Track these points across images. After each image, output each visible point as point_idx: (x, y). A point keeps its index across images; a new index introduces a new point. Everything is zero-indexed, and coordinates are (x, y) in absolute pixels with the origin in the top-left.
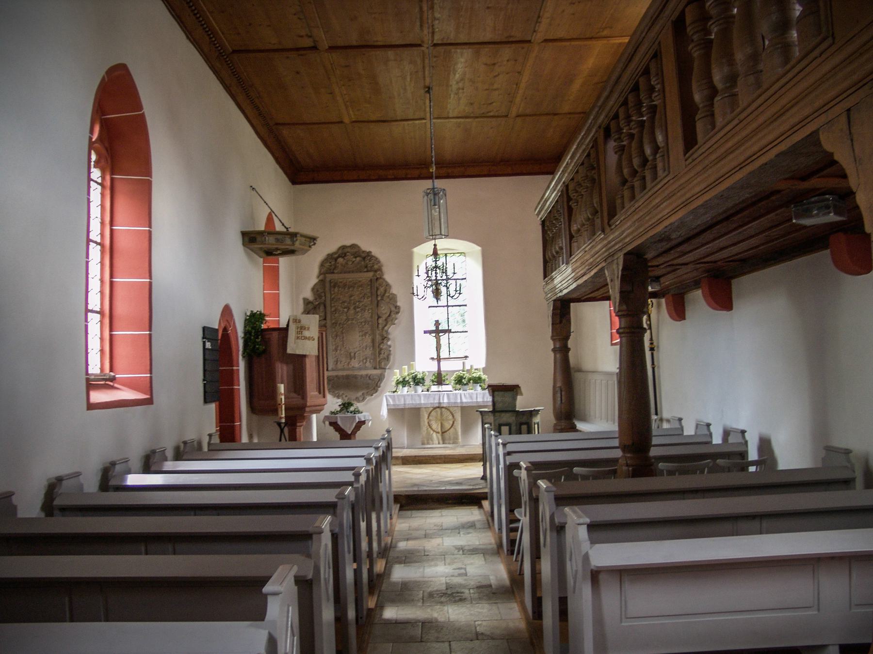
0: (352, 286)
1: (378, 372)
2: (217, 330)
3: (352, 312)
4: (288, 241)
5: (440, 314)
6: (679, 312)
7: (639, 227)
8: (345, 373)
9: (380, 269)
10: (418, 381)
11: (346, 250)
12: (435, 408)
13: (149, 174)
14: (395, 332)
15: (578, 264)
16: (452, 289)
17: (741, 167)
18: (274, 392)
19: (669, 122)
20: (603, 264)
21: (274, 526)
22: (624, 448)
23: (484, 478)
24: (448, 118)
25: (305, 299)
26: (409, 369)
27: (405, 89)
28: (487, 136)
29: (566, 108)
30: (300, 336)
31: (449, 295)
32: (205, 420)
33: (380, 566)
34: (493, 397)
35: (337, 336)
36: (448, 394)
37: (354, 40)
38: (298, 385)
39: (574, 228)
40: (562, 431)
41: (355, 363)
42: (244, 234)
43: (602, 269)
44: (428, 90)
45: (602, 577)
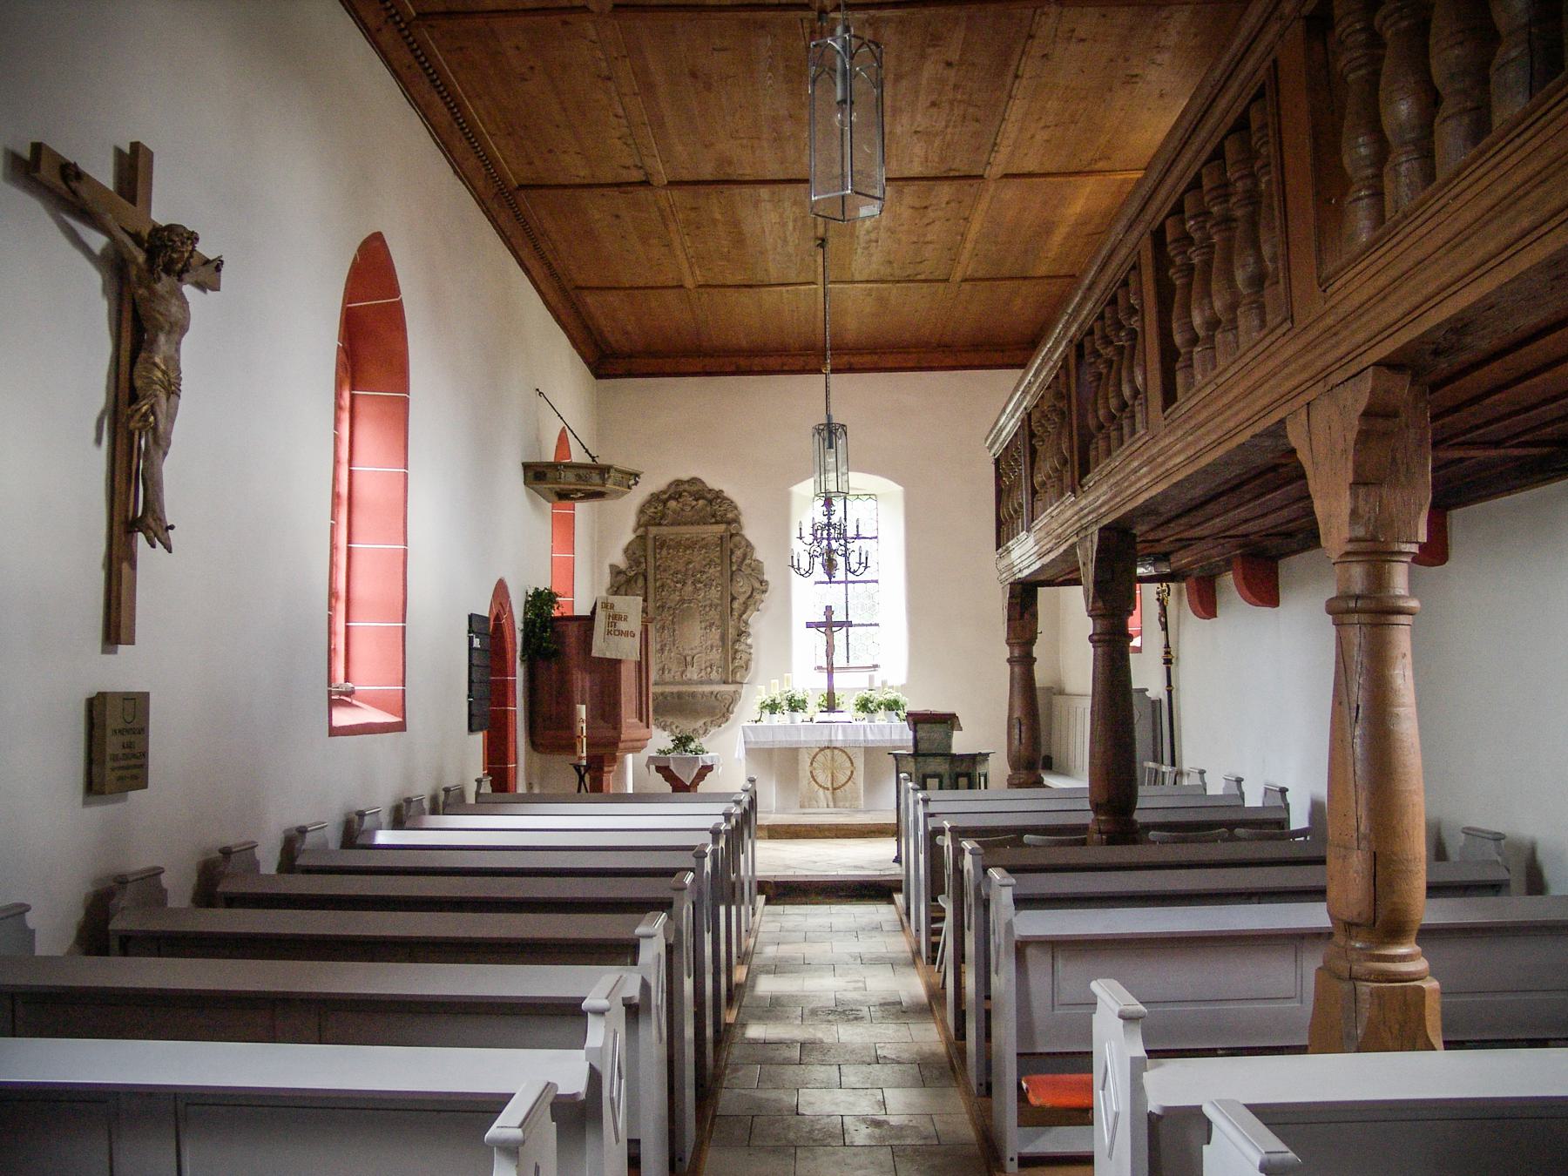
0: (691, 545)
1: (731, 688)
2: (487, 619)
3: (689, 588)
4: (596, 478)
5: (833, 595)
6: (1207, 606)
7: (1115, 496)
8: (675, 689)
9: (736, 520)
10: (795, 705)
11: (681, 488)
12: (822, 750)
13: (406, 390)
14: (760, 624)
15: (1043, 534)
16: (854, 559)
17: (1219, 443)
18: (569, 719)
19: (1290, 198)
20: (1075, 539)
21: (583, 910)
22: (1096, 807)
23: (897, 860)
24: (853, 282)
25: (612, 566)
26: (781, 684)
27: (785, 241)
28: (916, 308)
29: (1042, 270)
30: (613, 630)
31: (848, 570)
32: (467, 757)
33: (740, 974)
34: (915, 731)
35: (663, 628)
36: (849, 725)
37: (707, 172)
38: (607, 710)
39: (1038, 478)
40: (1019, 786)
41: (693, 673)
42: (527, 467)
43: (1073, 546)
44: (822, 242)
45: (1031, 952)
